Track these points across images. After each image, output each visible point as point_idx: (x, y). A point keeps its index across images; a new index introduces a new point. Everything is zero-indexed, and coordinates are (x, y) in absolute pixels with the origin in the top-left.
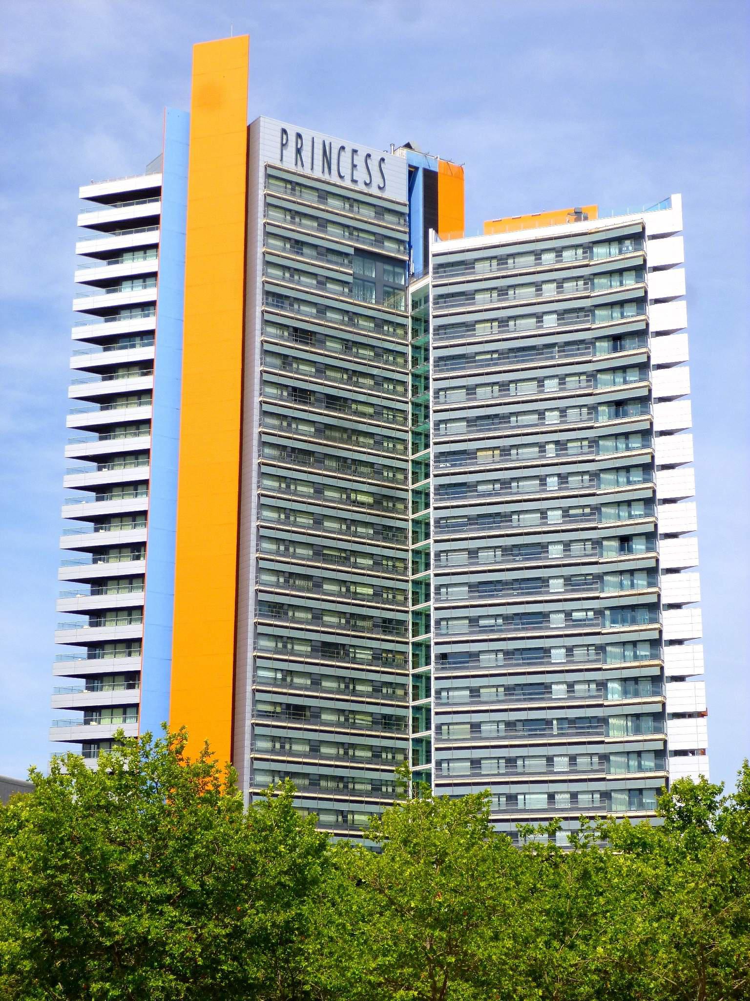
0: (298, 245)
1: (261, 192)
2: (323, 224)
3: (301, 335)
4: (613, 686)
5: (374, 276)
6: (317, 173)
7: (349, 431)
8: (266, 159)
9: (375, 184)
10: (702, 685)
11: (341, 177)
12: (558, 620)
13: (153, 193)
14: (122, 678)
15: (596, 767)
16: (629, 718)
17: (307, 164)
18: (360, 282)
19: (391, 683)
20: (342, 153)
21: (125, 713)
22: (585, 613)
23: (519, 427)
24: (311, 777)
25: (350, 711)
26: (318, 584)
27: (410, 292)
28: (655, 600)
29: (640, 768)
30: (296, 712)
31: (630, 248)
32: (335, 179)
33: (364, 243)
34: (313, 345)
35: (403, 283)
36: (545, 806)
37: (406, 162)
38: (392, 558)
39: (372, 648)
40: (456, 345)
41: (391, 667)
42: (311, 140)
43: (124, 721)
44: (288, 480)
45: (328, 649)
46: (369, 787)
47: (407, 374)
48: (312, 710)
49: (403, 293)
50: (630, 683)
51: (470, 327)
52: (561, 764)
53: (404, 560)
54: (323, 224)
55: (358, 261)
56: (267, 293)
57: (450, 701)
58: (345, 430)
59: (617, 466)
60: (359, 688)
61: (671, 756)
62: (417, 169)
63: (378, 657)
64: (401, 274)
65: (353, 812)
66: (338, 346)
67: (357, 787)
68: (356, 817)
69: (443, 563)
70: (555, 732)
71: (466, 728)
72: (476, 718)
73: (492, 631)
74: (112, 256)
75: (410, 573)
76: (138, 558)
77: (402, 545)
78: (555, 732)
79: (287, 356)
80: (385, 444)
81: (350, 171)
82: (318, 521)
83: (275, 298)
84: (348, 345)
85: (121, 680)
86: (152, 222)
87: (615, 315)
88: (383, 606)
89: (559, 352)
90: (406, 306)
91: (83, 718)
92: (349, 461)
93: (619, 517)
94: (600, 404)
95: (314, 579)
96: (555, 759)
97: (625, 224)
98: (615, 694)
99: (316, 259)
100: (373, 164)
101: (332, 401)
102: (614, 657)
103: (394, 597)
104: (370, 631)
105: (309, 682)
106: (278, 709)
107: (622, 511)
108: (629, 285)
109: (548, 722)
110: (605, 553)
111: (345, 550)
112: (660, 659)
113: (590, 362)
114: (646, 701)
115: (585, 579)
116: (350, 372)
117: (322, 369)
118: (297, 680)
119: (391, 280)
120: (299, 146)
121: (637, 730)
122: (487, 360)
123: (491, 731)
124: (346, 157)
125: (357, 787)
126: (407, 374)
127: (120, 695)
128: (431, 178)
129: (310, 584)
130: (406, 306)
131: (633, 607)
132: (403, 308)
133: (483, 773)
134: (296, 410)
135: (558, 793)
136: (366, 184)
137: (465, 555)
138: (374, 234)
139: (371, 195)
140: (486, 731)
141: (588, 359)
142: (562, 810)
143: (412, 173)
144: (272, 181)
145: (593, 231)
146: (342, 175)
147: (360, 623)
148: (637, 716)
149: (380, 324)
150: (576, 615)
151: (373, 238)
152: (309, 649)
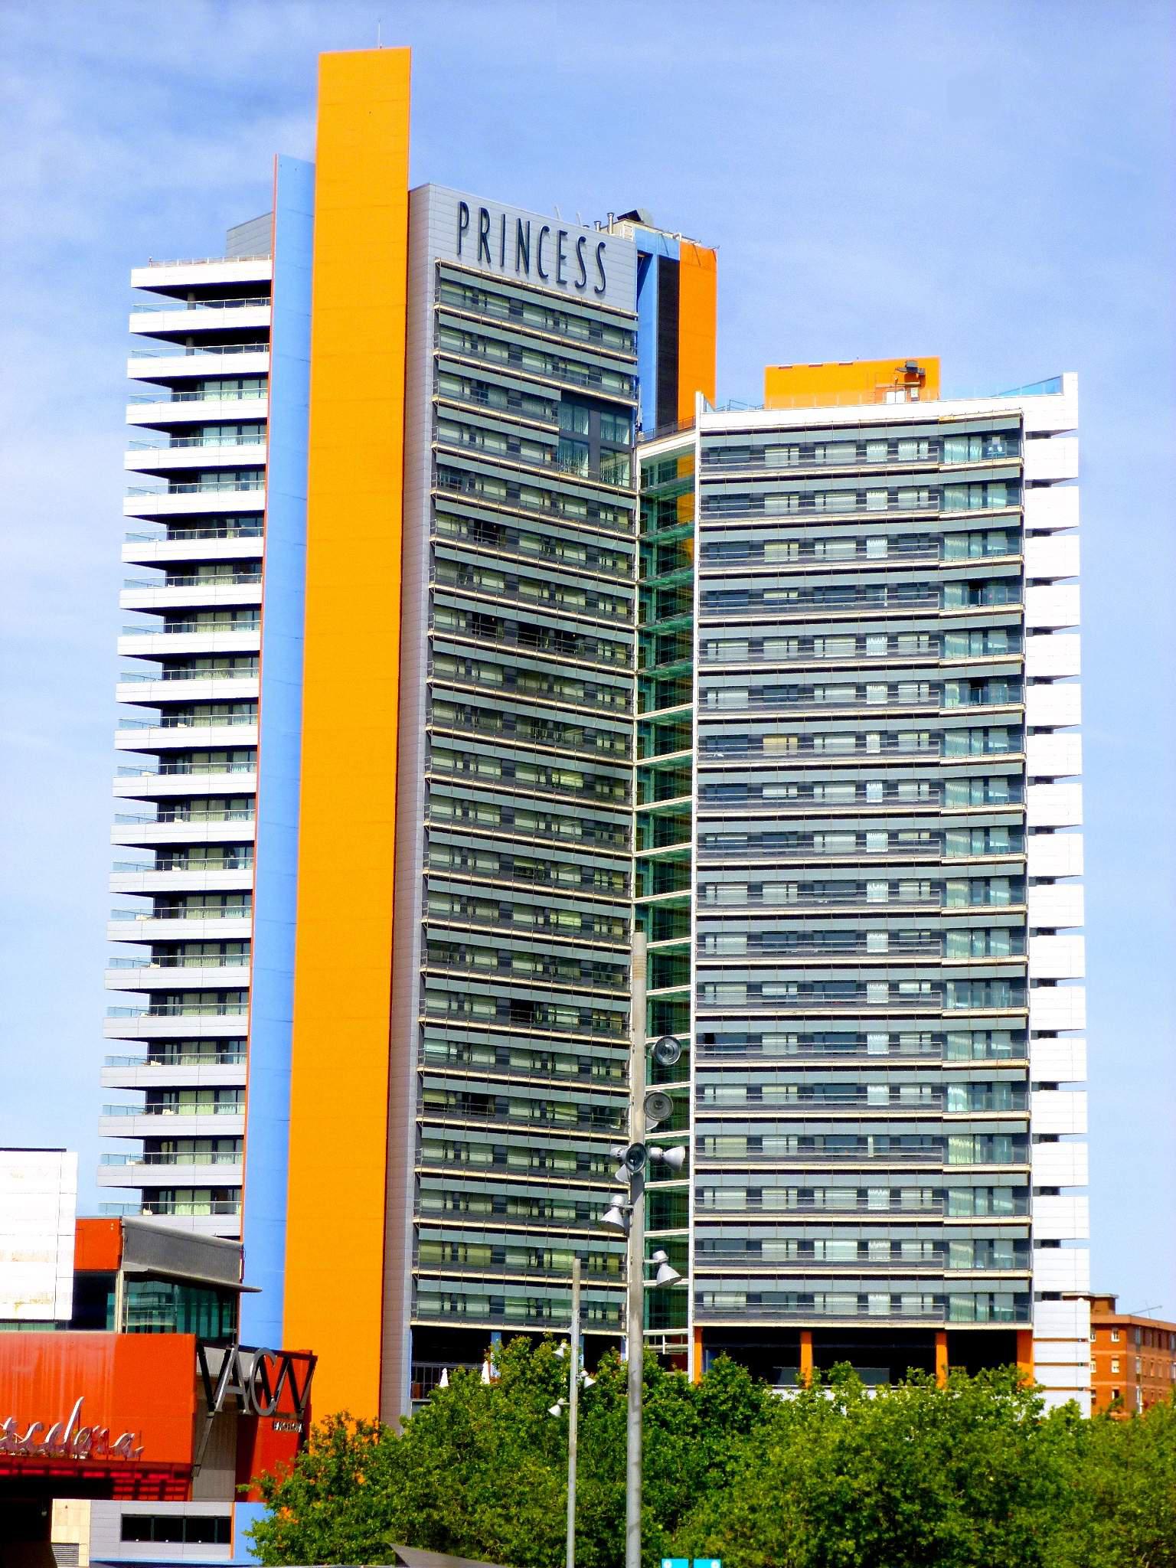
0: (481, 390)
2: (516, 354)
3: (486, 532)
5: (586, 432)
6: (509, 275)
7: (551, 679)
8: (438, 253)
9: (590, 286)
11: (543, 276)
12: (877, 993)
13: (257, 291)
14: (230, 568)
15: (929, 1206)
16: (978, 1138)
17: (495, 258)
18: (569, 442)
19: (604, 1060)
20: (545, 239)
21: (217, 1099)
22: (917, 986)
23: (828, 706)
24: (496, 1199)
25: (548, 1102)
27: (638, 459)
28: (1022, 974)
29: (991, 1210)
30: (476, 1105)
31: (1000, 449)
32: (533, 281)
33: (572, 381)
34: (503, 549)
35: (626, 442)
36: (854, 1258)
37: (633, 246)
38: (608, 871)
39: (579, 1008)
40: (736, 575)
41: (604, 1033)
42: (500, 218)
43: (216, 1111)
44: (467, 757)
45: (522, 1011)
46: (573, 1214)
47: (632, 587)
48: (497, 1101)
49: (626, 457)
50: (980, 1090)
51: (756, 548)
52: (878, 1199)
53: (624, 874)
54: (516, 354)
55: (566, 411)
56: (439, 467)
57: (718, 1103)
58: (544, 676)
59: (972, 774)
60: (560, 1067)
61: (1030, 834)
62: (649, 256)
63: (586, 1020)
64: (623, 428)
65: (550, 1251)
66: (536, 546)
67: (557, 1213)
68: (556, 1257)
69: (710, 901)
70: (871, 1154)
71: (740, 1144)
72: (756, 1129)
73: (782, 1005)
74: (185, 386)
75: (633, 894)
77: (621, 850)
78: (871, 1154)
79: (465, 565)
80: (600, 697)
81: (554, 267)
82: (507, 817)
83: (452, 477)
84: (550, 543)
85: (210, 1049)
86: (256, 337)
88: (595, 944)
89: (889, 598)
90: (632, 479)
92: (551, 725)
95: (501, 905)
96: (870, 1192)
97: (995, 414)
98: (958, 1104)
99: (506, 410)
101: (529, 634)
103: (610, 930)
104: (576, 981)
105: (493, 1060)
106: (452, 1101)
107: (976, 840)
108: (998, 506)
109: (862, 1140)
110: (949, 902)
111: (544, 861)
113: (936, 617)
114: (1000, 1116)
115: (920, 937)
116: (553, 587)
117: (513, 584)
118: (477, 1058)
120: (484, 231)
121: (990, 1158)
122: (782, 602)
123: (777, 1149)
124: (550, 243)
125: (557, 1213)
126: (632, 587)
128: (670, 270)
129: (576, 972)
130: (632, 479)
131: (988, 982)
132: (626, 483)
133: (764, 1208)
134: (477, 646)
135: (872, 1240)
136: (577, 286)
137: (743, 890)
138: (588, 366)
140: (770, 1148)
141: (935, 760)
142: (879, 1265)
143: (644, 259)
144: (446, 288)
145: (946, 419)
146: (545, 273)
147: (562, 970)
148: (990, 1137)
149: (594, 510)
150: (905, 988)
151: (586, 372)
152: (493, 1010)
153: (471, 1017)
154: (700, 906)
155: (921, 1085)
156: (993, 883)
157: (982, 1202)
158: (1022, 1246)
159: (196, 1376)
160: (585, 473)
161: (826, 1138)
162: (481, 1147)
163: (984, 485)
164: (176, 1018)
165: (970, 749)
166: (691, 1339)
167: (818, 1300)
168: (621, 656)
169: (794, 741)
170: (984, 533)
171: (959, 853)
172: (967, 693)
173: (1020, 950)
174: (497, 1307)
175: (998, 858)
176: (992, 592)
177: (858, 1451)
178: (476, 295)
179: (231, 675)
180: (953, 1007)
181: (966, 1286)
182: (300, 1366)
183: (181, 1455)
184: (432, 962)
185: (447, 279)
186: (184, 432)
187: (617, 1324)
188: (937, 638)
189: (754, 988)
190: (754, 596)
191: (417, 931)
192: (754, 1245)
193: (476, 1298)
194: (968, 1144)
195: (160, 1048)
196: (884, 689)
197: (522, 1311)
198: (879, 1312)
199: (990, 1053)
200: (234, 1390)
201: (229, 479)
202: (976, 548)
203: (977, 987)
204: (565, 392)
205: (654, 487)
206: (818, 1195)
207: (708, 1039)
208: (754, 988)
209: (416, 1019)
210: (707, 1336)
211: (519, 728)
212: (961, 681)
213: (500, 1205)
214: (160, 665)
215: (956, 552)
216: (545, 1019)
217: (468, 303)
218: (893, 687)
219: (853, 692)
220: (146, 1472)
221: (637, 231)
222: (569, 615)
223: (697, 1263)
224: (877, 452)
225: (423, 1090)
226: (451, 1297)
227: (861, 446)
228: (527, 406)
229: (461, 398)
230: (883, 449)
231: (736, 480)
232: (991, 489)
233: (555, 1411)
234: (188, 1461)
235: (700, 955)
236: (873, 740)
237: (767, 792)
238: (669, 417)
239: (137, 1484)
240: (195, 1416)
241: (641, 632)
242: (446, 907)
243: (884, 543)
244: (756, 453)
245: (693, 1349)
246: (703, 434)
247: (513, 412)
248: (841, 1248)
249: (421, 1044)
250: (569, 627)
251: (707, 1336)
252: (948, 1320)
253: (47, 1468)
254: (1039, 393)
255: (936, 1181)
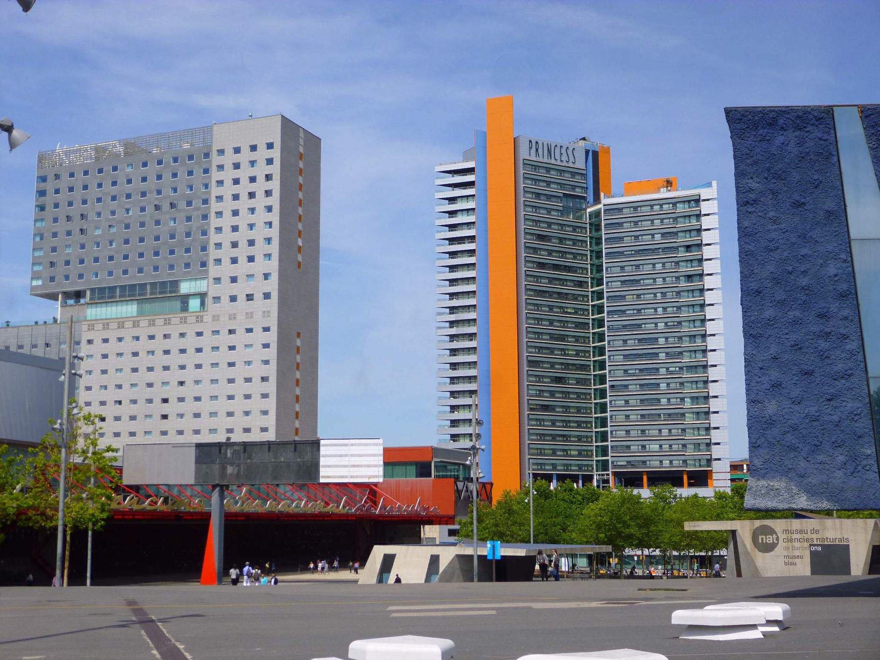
0: (538, 195)
1: (521, 172)
2: (548, 183)
3: (541, 237)
4: (688, 400)
6: (545, 160)
9: (570, 161)
10: (726, 400)
13: (471, 171)
17: (541, 156)
26: (551, 351)
30: (545, 408)
32: (553, 161)
33: (566, 190)
36: (658, 450)
40: (616, 247)
45: (559, 380)
50: (695, 399)
52: (665, 432)
54: (548, 183)
55: (564, 199)
58: (561, 279)
70: (662, 419)
72: (628, 413)
73: (634, 376)
74: (452, 200)
76: (471, 340)
84: (561, 240)
86: (471, 184)
87: (686, 221)
91: (449, 410)
93: (690, 327)
94: (681, 276)
98: (688, 403)
100: (570, 152)
101: (556, 267)
102: (688, 387)
109: (659, 415)
112: (707, 389)
117: (550, 253)
119: (579, 206)
122: (629, 255)
127: (467, 401)
128: (595, 154)
130: (586, 218)
131: (696, 367)
132: (584, 220)
139: (569, 167)
143: (587, 152)
148: (698, 413)
150: (671, 369)
153: (543, 382)
154: (608, 347)
155: (677, 398)
156: (696, 337)
157: (696, 432)
158: (708, 445)
159: (455, 491)
160: (571, 218)
161: (649, 415)
162: (548, 420)
163: (689, 216)
164: (457, 385)
165: (688, 297)
166: (610, 475)
167: (648, 462)
168: (585, 272)
169: (635, 296)
170: (690, 231)
171: (686, 329)
172: (686, 279)
173: (705, 357)
174: (554, 467)
175: (698, 329)
176: (693, 249)
177: (605, 510)
178: (535, 167)
179: (468, 284)
180: (686, 375)
181: (691, 457)
182: (488, 487)
183: (451, 512)
184: (530, 366)
185: (527, 163)
186: (452, 213)
187: (592, 471)
188: (677, 263)
189: (626, 371)
190: (621, 253)
191: (525, 358)
192: (628, 447)
193: (547, 464)
194: (691, 415)
195: (453, 394)
196: (661, 279)
197: (562, 468)
198: (666, 466)
199: (697, 388)
200: (467, 494)
201: (465, 227)
202: (688, 236)
203: (692, 368)
204: (564, 193)
205: (593, 220)
206: (647, 432)
207: (612, 386)
208: (626, 371)
209: (526, 383)
210: (615, 474)
211: (554, 296)
212: (684, 276)
213: (554, 437)
214: (448, 282)
215: (682, 237)
216: (566, 382)
217: (533, 170)
218: (664, 279)
219: (652, 281)
220: (441, 518)
221: (585, 143)
222: (569, 261)
223: (611, 453)
224: (657, 208)
225: (529, 404)
226: (541, 464)
227: (652, 206)
228: (553, 199)
229: (532, 198)
230: (658, 207)
231: (615, 218)
232: (691, 217)
233: (526, 501)
234: (453, 514)
235: (609, 362)
236: (659, 295)
237: (627, 312)
238: (597, 200)
239: (440, 521)
240: (455, 501)
241: (590, 264)
242: (534, 350)
243: (660, 235)
244: (620, 210)
245: (611, 478)
246: (604, 205)
247: (549, 201)
248: (655, 447)
249: (528, 391)
250: (568, 264)
251: (615, 474)
252: (687, 467)
253: (411, 517)
254: (705, 187)
255: (682, 426)
